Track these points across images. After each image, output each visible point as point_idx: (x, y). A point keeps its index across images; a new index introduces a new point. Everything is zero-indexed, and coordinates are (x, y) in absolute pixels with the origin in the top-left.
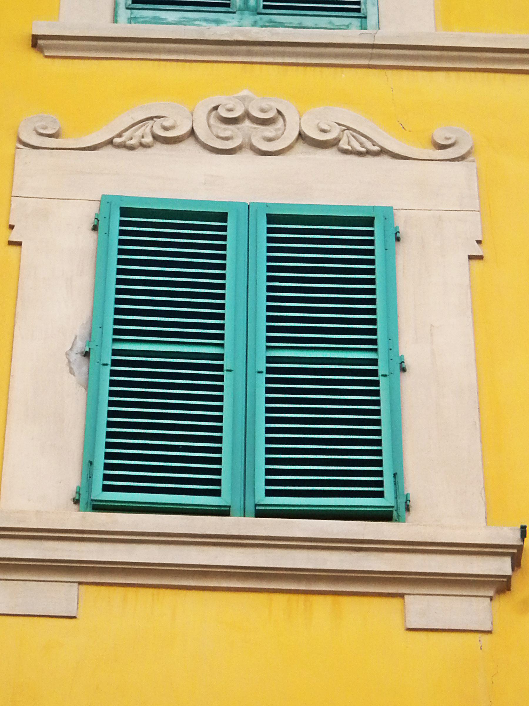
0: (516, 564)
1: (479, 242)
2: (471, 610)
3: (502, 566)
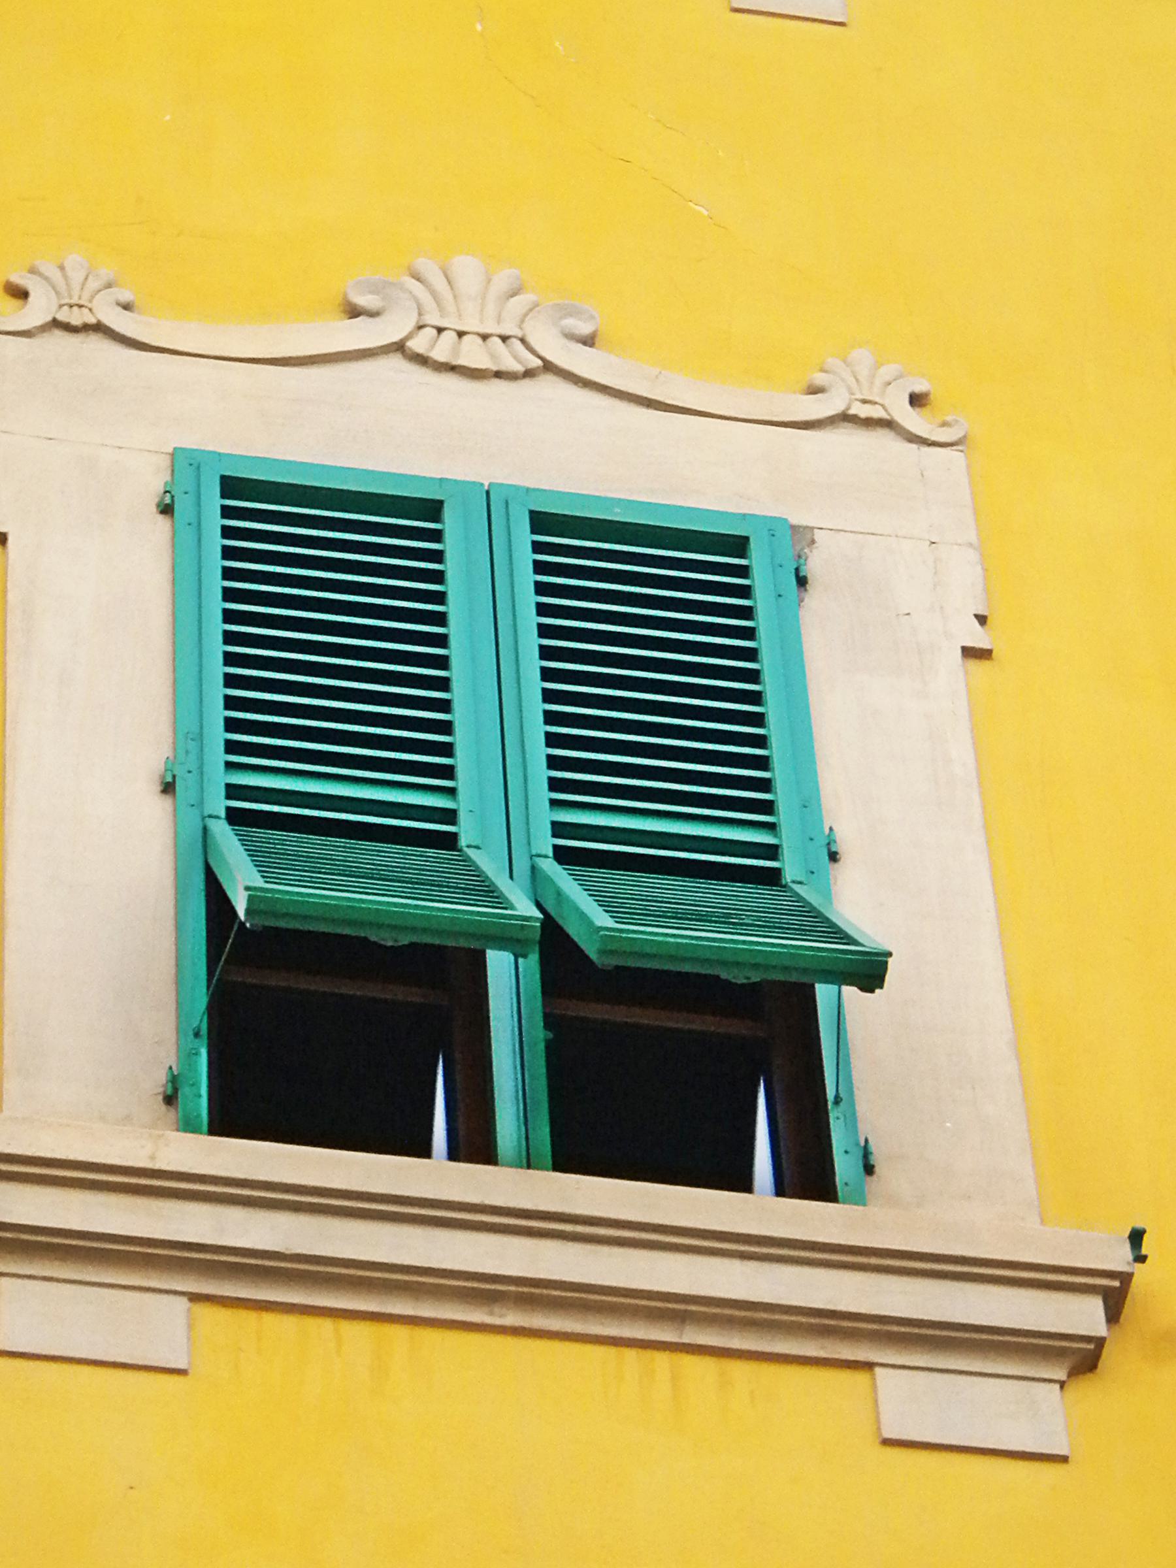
0: (1113, 1315)
3: (1083, 1316)
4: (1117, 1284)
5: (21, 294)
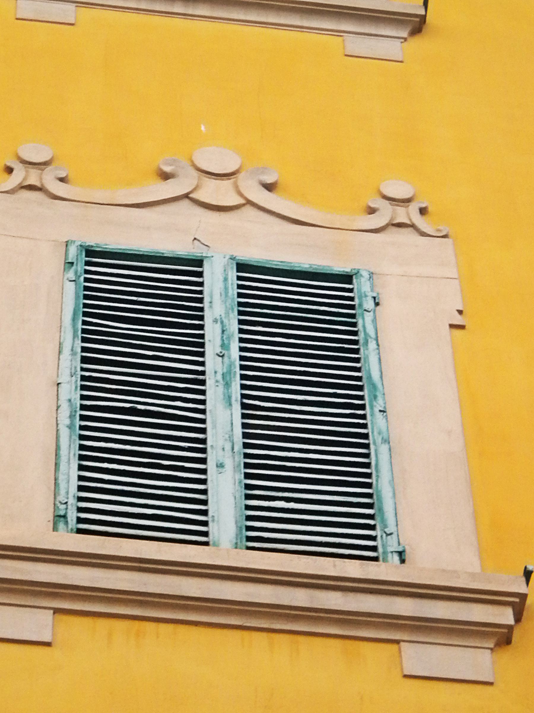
0: (518, 619)
1: (460, 312)
3: (505, 616)
4: (517, 600)
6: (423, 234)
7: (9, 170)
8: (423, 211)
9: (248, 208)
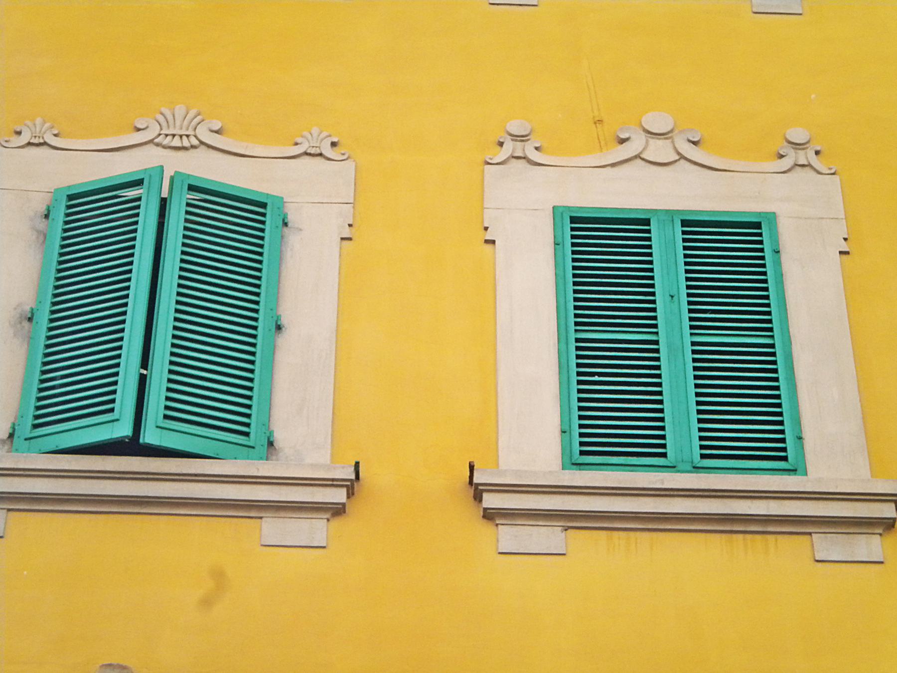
0: (350, 494)
1: (845, 239)
2: (315, 528)
3: (339, 496)
4: (349, 483)
5: (19, 133)
6: (329, 159)
7: (501, 144)
8: (817, 153)
9: (682, 161)
